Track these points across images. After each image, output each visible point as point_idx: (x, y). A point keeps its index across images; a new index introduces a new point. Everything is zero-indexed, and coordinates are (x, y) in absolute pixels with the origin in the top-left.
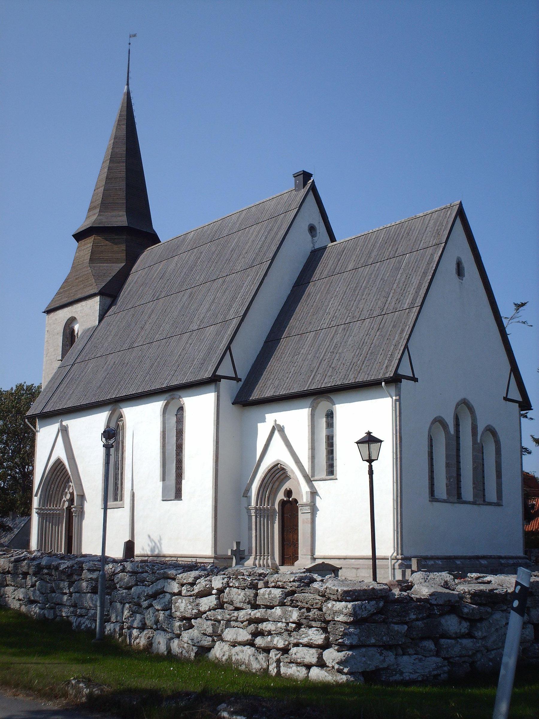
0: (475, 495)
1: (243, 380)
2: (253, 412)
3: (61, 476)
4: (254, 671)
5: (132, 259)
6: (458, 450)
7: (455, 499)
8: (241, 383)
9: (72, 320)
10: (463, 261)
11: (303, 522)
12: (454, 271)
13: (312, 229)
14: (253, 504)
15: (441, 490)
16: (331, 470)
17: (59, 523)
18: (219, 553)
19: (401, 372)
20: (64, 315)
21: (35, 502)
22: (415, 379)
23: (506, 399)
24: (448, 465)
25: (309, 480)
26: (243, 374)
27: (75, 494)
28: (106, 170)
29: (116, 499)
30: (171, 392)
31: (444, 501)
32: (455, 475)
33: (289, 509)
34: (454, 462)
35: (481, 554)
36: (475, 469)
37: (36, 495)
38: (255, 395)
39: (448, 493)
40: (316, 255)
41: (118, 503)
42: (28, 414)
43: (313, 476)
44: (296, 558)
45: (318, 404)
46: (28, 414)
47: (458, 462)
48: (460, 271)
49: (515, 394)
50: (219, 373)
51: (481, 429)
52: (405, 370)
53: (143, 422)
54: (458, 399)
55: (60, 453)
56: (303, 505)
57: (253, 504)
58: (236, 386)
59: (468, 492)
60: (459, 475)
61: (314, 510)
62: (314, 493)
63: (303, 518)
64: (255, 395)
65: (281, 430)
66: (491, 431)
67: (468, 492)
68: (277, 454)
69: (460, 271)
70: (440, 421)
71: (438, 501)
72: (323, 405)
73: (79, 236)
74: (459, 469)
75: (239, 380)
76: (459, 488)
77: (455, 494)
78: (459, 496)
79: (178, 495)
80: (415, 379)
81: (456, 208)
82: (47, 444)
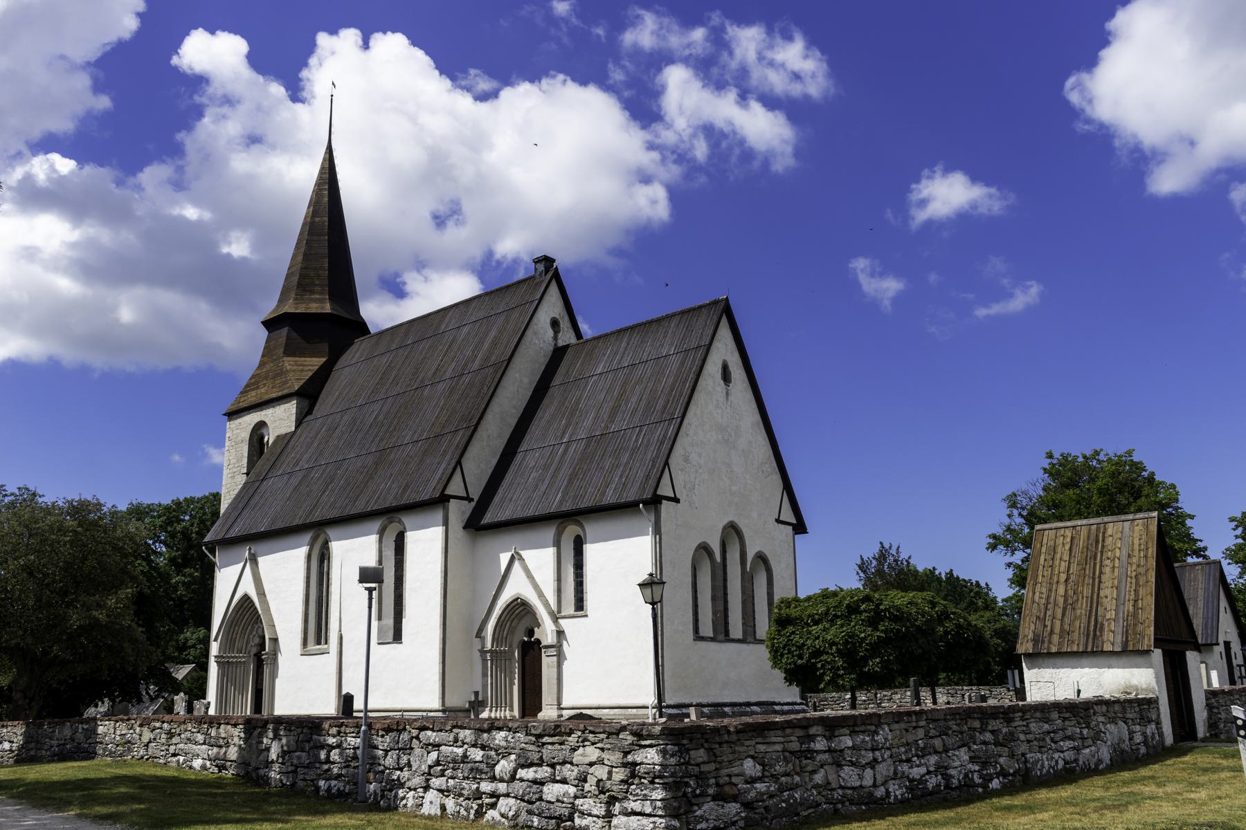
0: (745, 632)
1: (476, 499)
2: (489, 543)
3: (247, 615)
4: (652, 203)
5: (335, 356)
6: (725, 580)
7: (721, 637)
8: (473, 504)
9: (261, 425)
10: (730, 365)
11: (548, 666)
12: (719, 376)
13: (555, 324)
14: (489, 646)
15: (707, 629)
16: (580, 604)
17: (243, 691)
18: (448, 704)
19: (659, 492)
20: (251, 419)
21: (214, 648)
22: (676, 500)
23: (778, 521)
24: (714, 599)
25: (555, 619)
26: (475, 494)
27: (267, 637)
28: (300, 258)
29: (319, 643)
30: (390, 517)
31: (712, 639)
32: (722, 608)
33: (531, 651)
34: (721, 594)
35: (753, 700)
36: (744, 602)
37: (216, 640)
38: (487, 519)
39: (715, 630)
40: (559, 353)
41: (323, 647)
42: (206, 540)
43: (559, 612)
44: (539, 709)
45: (565, 528)
46: (206, 540)
47: (726, 594)
48: (726, 376)
49: (788, 516)
50: (448, 492)
51: (750, 555)
52: (665, 490)
53: (355, 551)
54: (725, 522)
55: (247, 587)
56: (547, 647)
57: (489, 646)
58: (468, 507)
59: (736, 630)
60: (726, 610)
61: (560, 657)
62: (560, 633)
63: (548, 663)
64: (487, 519)
65: (521, 559)
66: (762, 558)
67: (736, 630)
68: (517, 586)
69: (726, 376)
70: (704, 548)
71: (703, 639)
72: (572, 530)
73: (270, 324)
74: (726, 602)
75: (470, 500)
76: (726, 624)
77: (722, 633)
78: (727, 633)
79: (397, 637)
80: (676, 500)
81: (723, 304)
82: (228, 583)
